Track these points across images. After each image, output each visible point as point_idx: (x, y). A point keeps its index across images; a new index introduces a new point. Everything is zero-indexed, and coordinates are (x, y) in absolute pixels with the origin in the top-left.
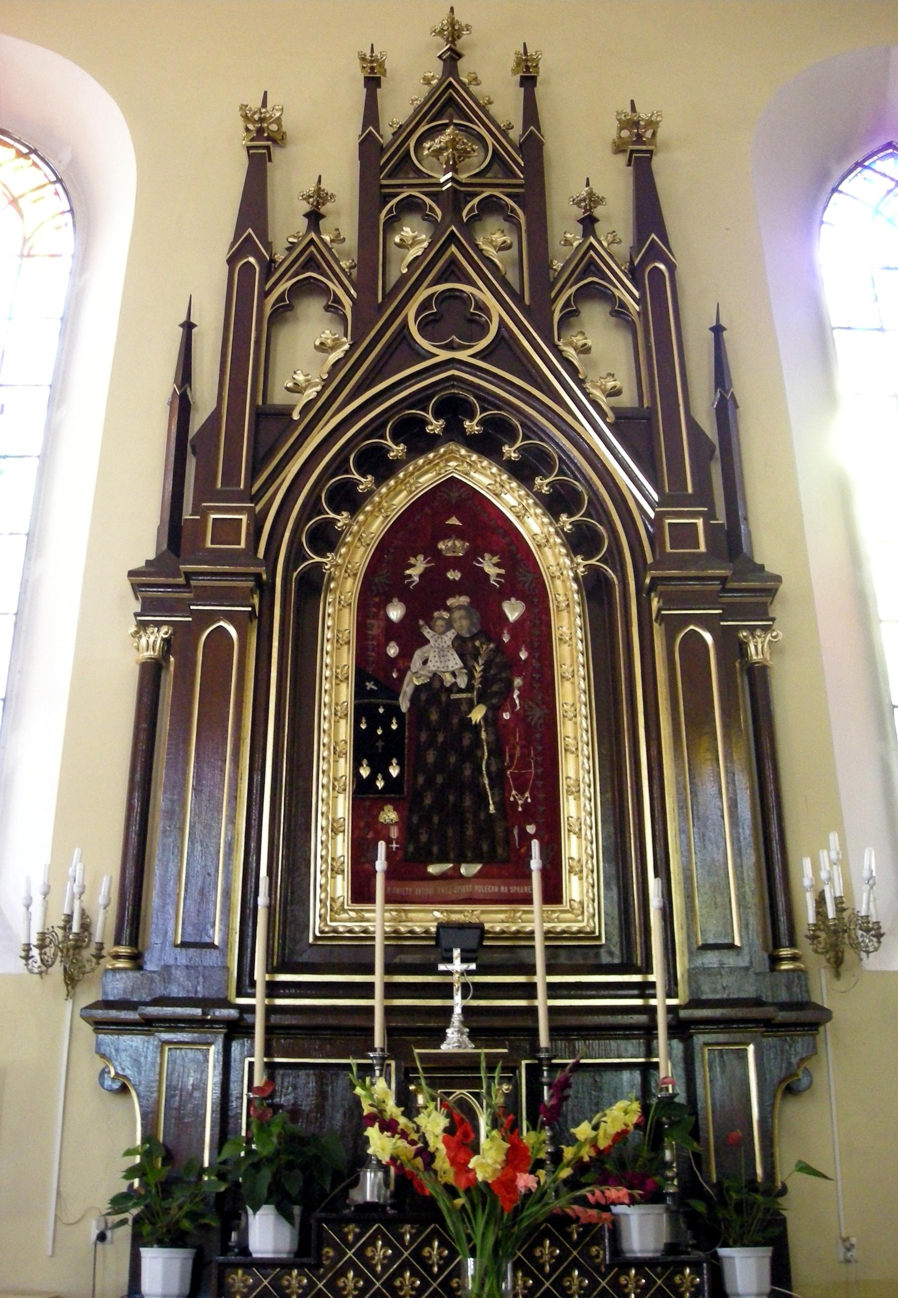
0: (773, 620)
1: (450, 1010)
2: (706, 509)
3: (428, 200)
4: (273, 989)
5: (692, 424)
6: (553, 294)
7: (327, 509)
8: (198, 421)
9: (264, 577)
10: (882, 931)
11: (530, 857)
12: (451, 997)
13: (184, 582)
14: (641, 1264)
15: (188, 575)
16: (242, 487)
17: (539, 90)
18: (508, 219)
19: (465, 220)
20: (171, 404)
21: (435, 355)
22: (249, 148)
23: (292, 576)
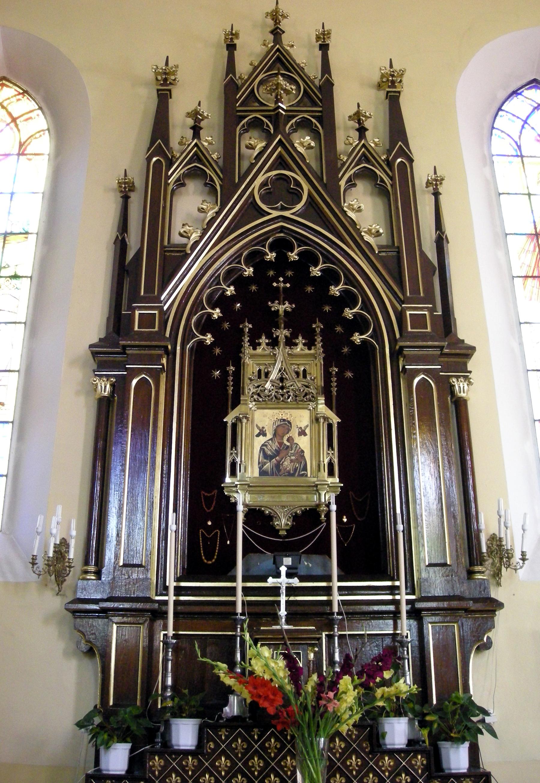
0: (470, 372)
1: (278, 603)
2: (431, 306)
3: (314, 120)
4: (179, 591)
5: (422, 253)
6: (340, 176)
7: (206, 306)
8: (131, 254)
9: (170, 347)
10: (527, 557)
11: (337, 511)
12: (279, 595)
13: (122, 351)
14: (392, 753)
15: (124, 347)
16: (422, 295)
17: (330, 53)
18: (264, 130)
19: (287, 132)
20: (115, 243)
21: (269, 214)
22: (158, 90)
23: (186, 348)
